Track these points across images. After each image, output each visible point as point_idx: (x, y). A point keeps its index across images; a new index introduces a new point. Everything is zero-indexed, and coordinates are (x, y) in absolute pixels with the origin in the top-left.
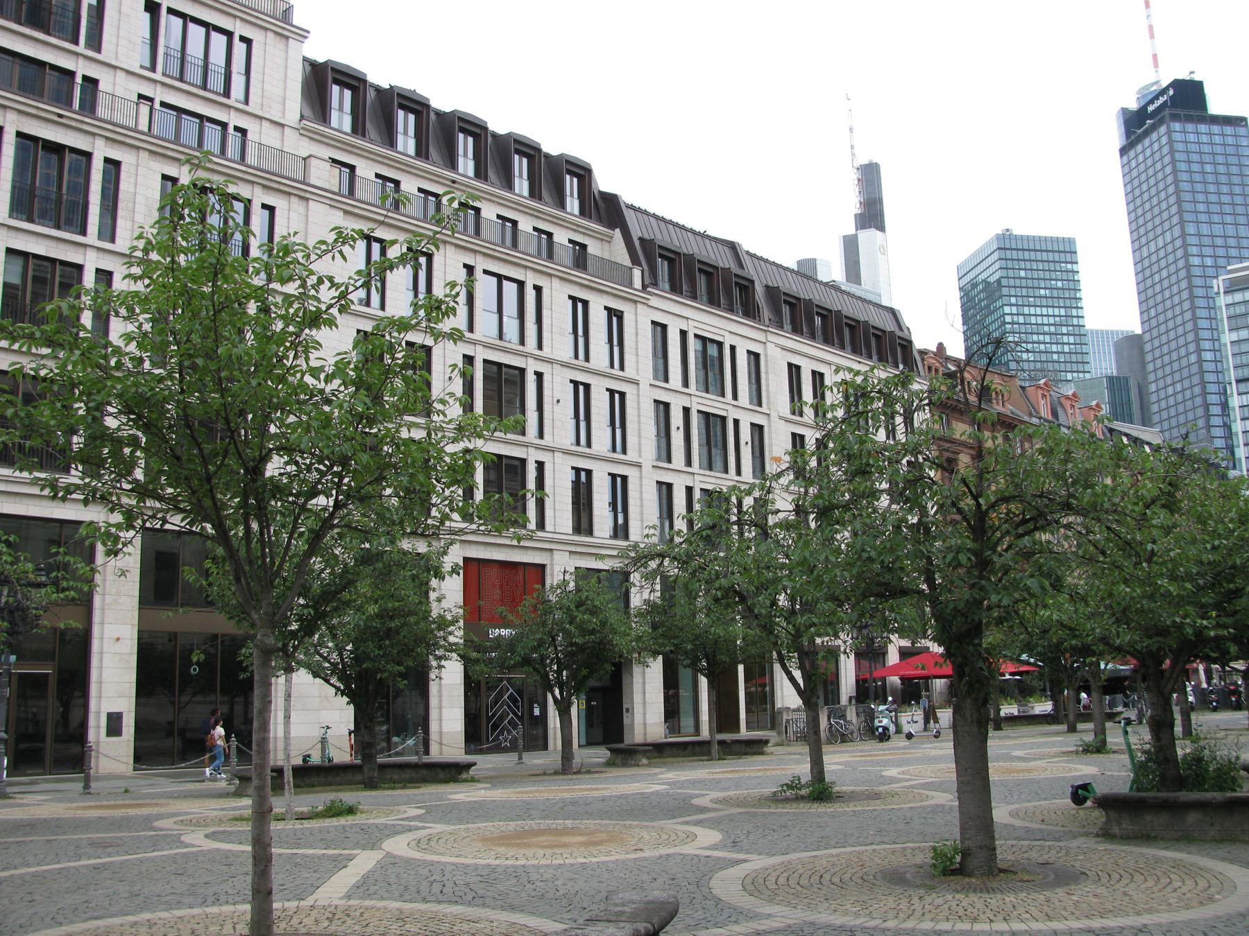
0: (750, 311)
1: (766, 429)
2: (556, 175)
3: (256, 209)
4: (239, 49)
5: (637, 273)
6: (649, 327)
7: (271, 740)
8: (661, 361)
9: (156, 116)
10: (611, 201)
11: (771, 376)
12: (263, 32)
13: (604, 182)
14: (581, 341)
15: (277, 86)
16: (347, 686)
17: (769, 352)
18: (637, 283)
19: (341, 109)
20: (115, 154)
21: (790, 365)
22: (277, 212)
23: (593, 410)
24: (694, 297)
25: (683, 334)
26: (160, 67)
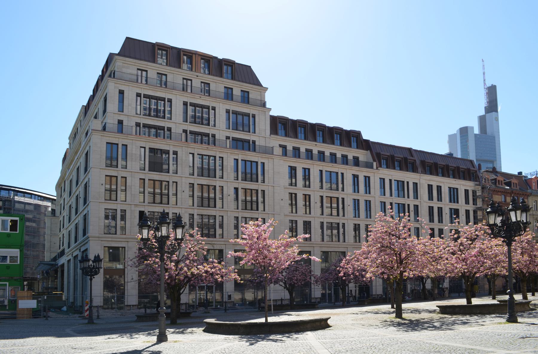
0: (414, 170)
1: (419, 206)
2: (351, 138)
3: (217, 158)
4: (212, 112)
5: (375, 164)
6: (378, 180)
7: (374, 288)
8: (383, 190)
9: (141, 129)
10: (367, 141)
11: (421, 189)
12: (128, 87)
13: (365, 137)
14: (368, 188)
15: (263, 125)
16: (286, 286)
17: (421, 182)
18: (375, 167)
19: (301, 133)
20: (263, 161)
21: (429, 185)
22: (224, 159)
23: (360, 207)
24: (394, 169)
25: (390, 180)
26: (231, 128)
